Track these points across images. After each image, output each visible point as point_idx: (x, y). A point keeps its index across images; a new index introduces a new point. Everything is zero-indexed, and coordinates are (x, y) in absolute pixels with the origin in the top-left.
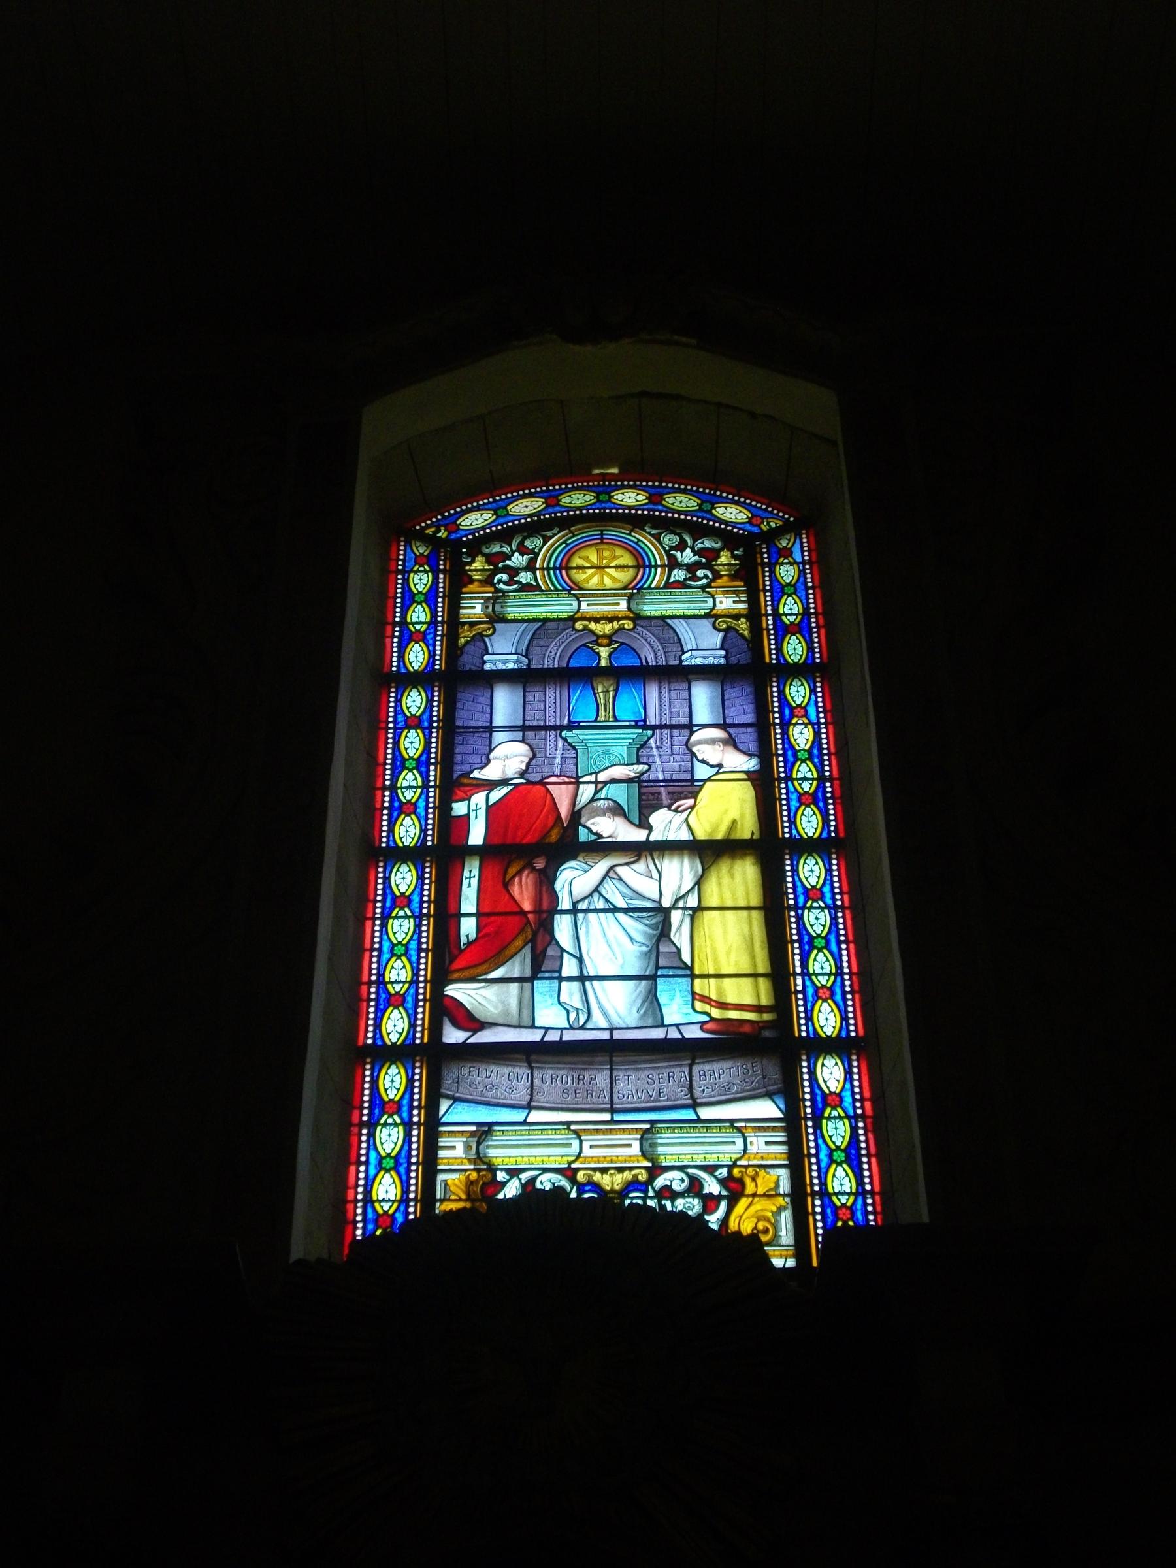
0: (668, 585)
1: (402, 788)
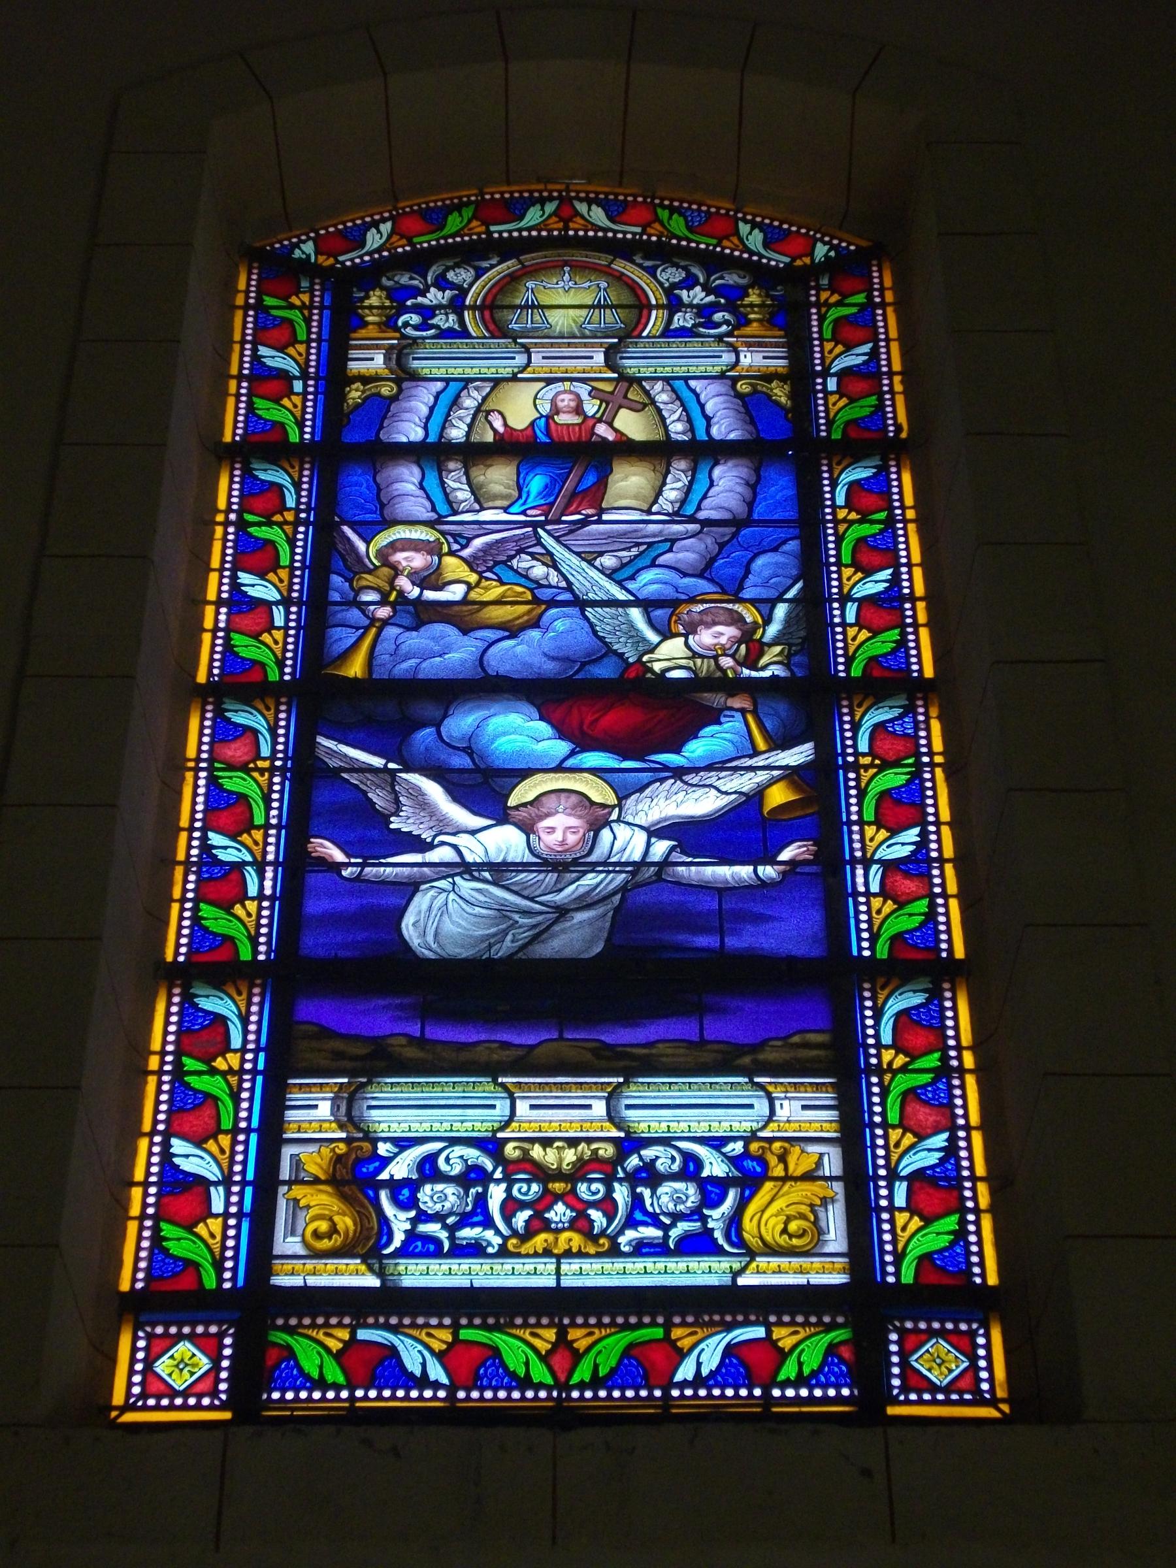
0: (667, 332)
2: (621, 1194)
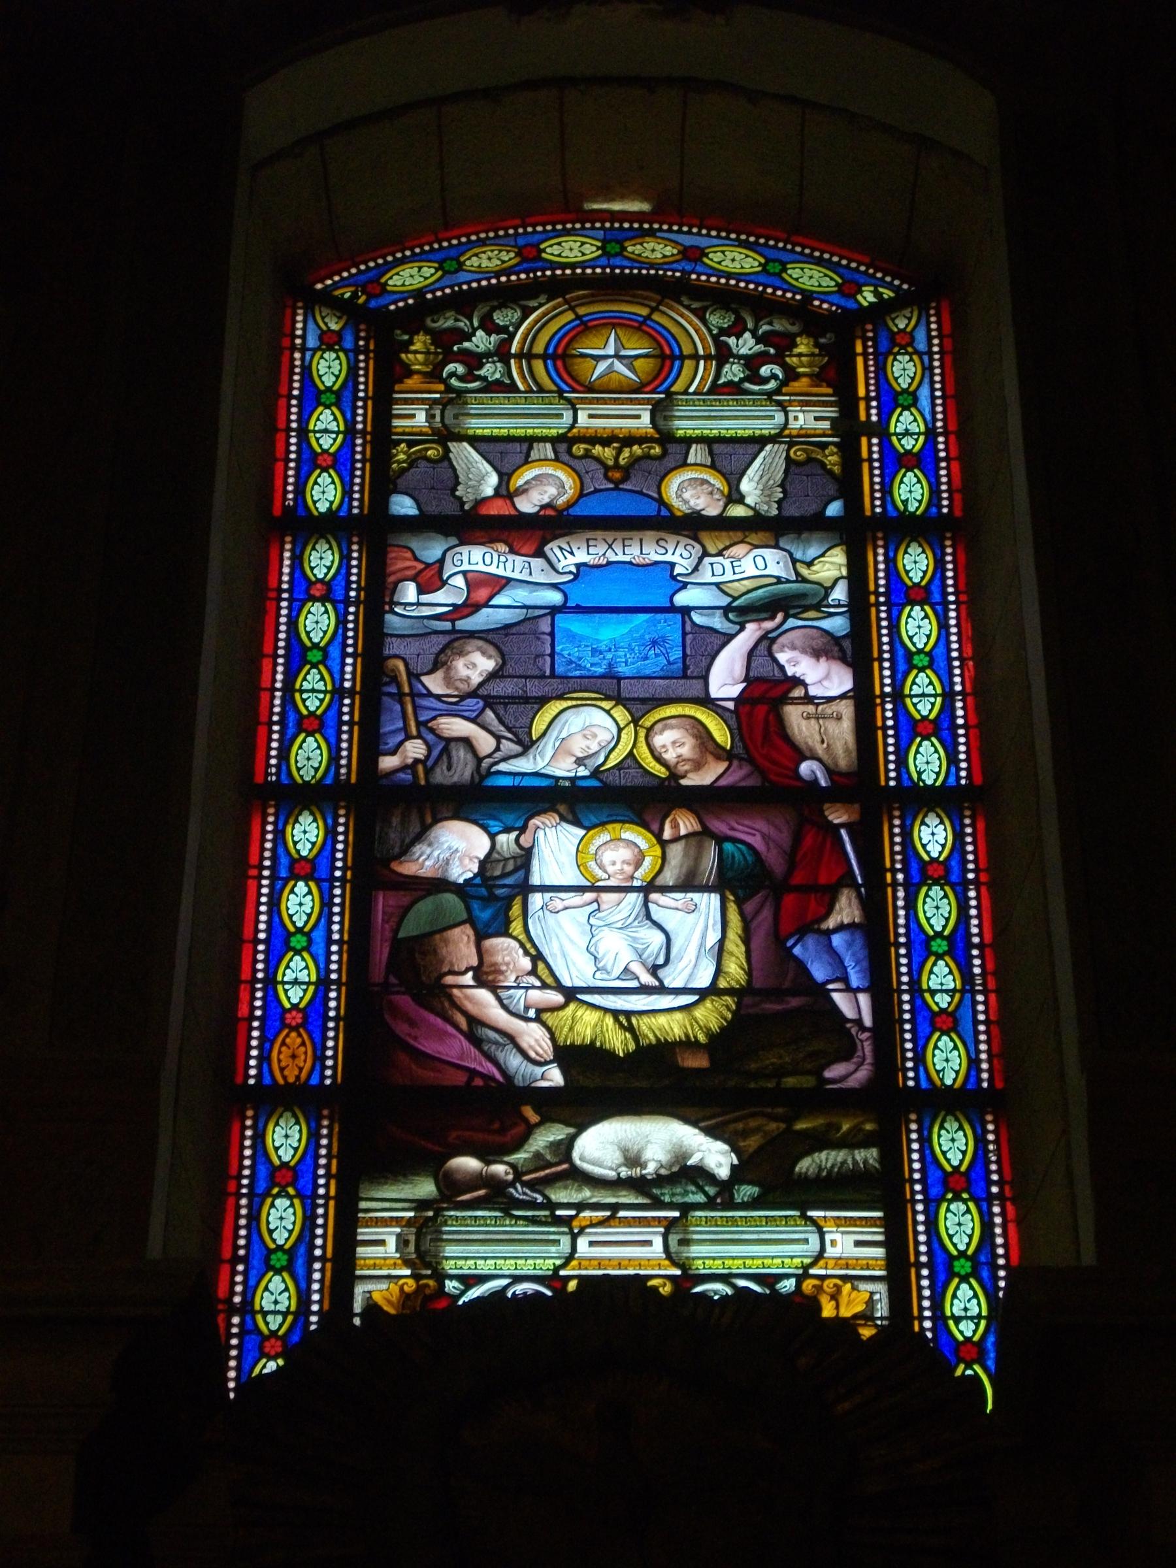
0: (715, 389)
1: (315, 432)
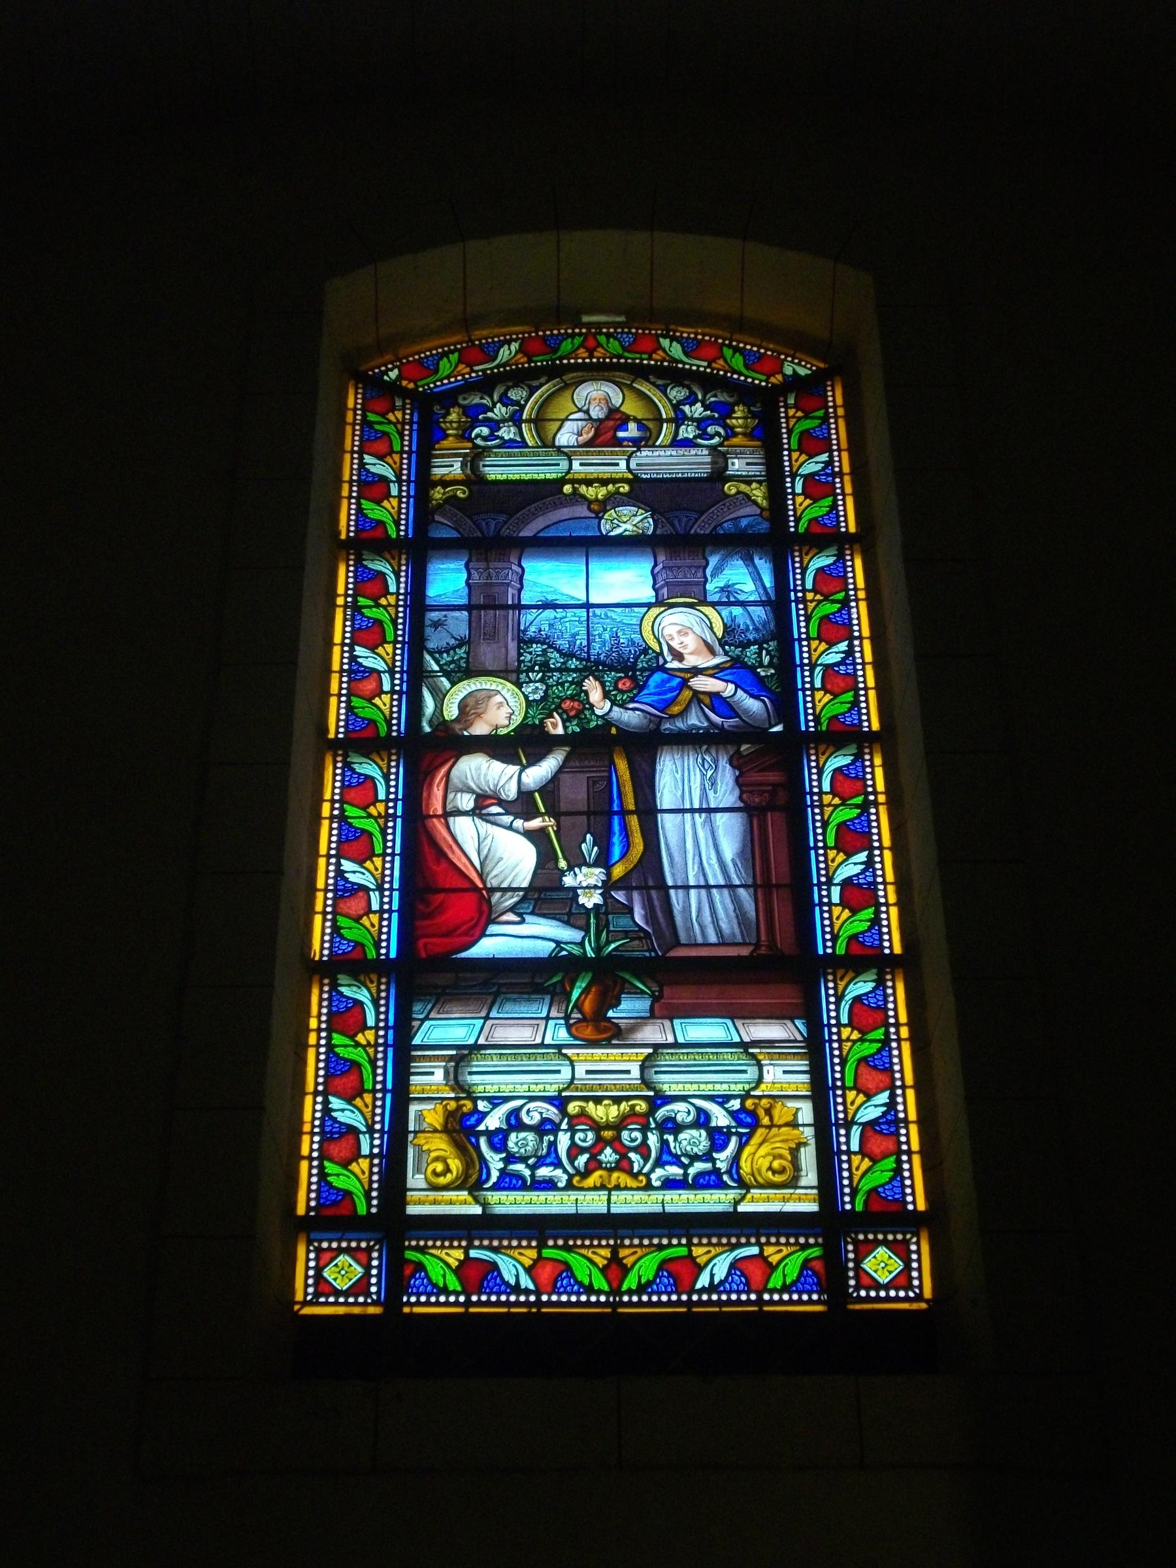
2: (653, 1140)
